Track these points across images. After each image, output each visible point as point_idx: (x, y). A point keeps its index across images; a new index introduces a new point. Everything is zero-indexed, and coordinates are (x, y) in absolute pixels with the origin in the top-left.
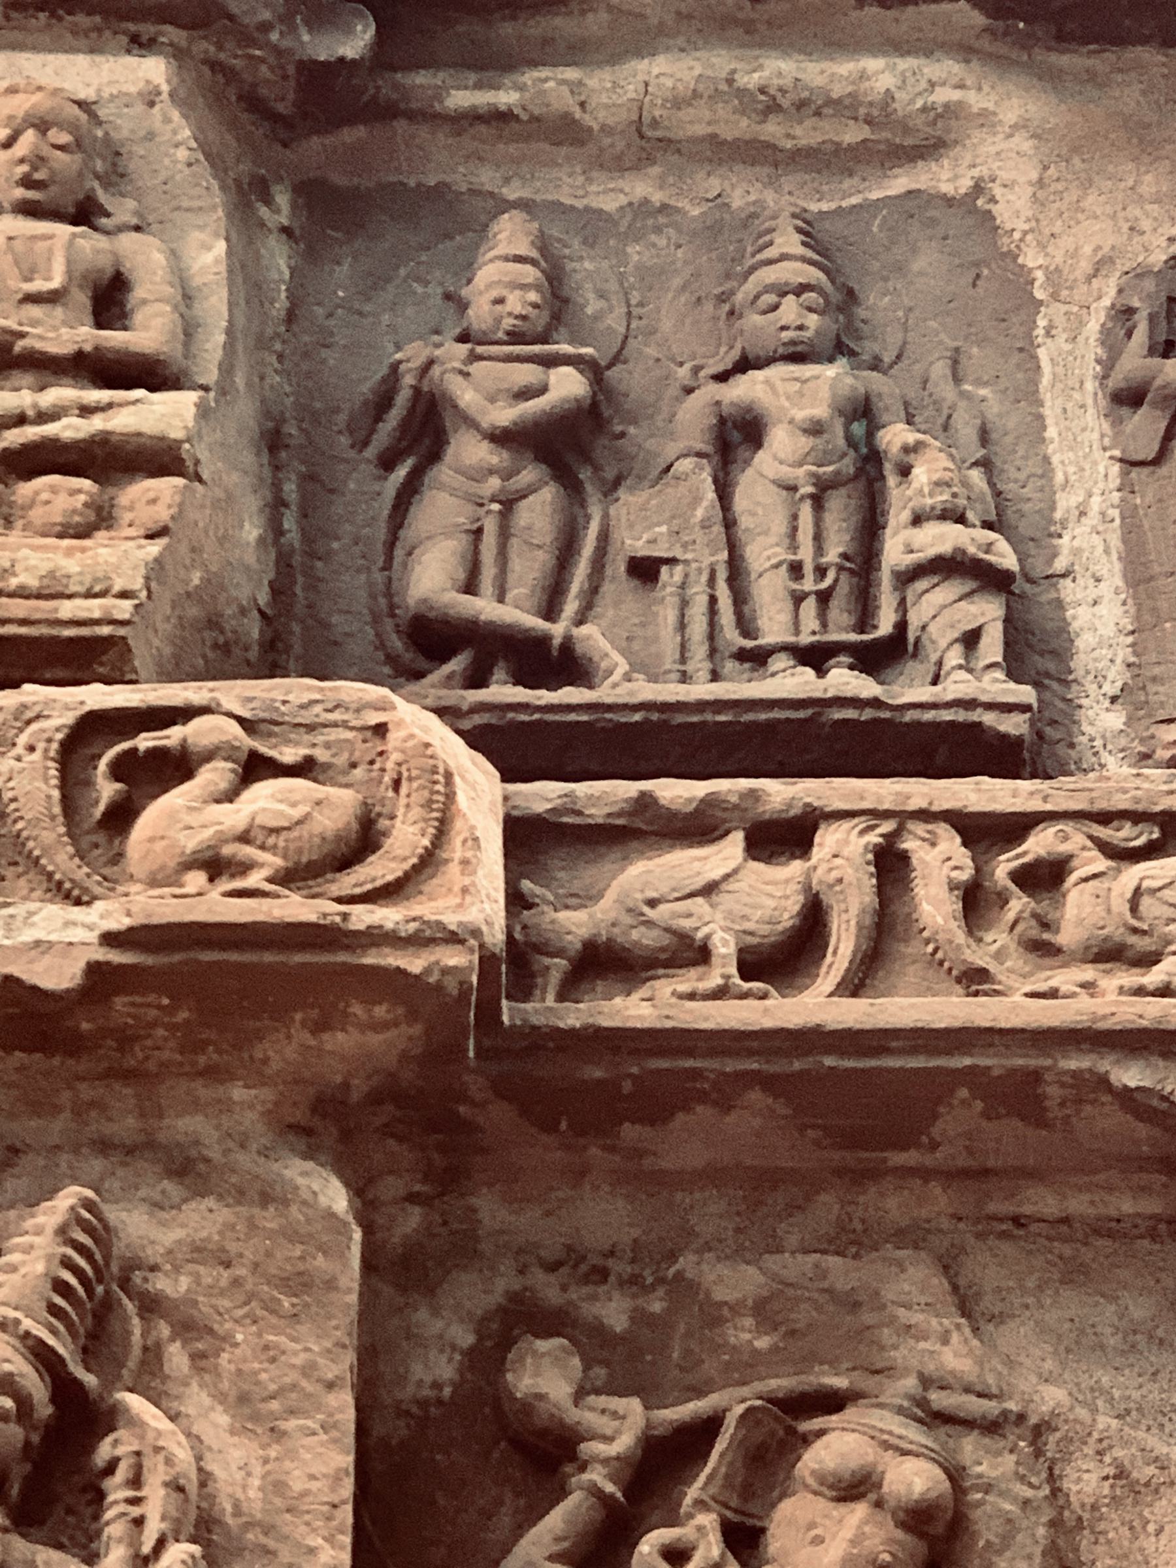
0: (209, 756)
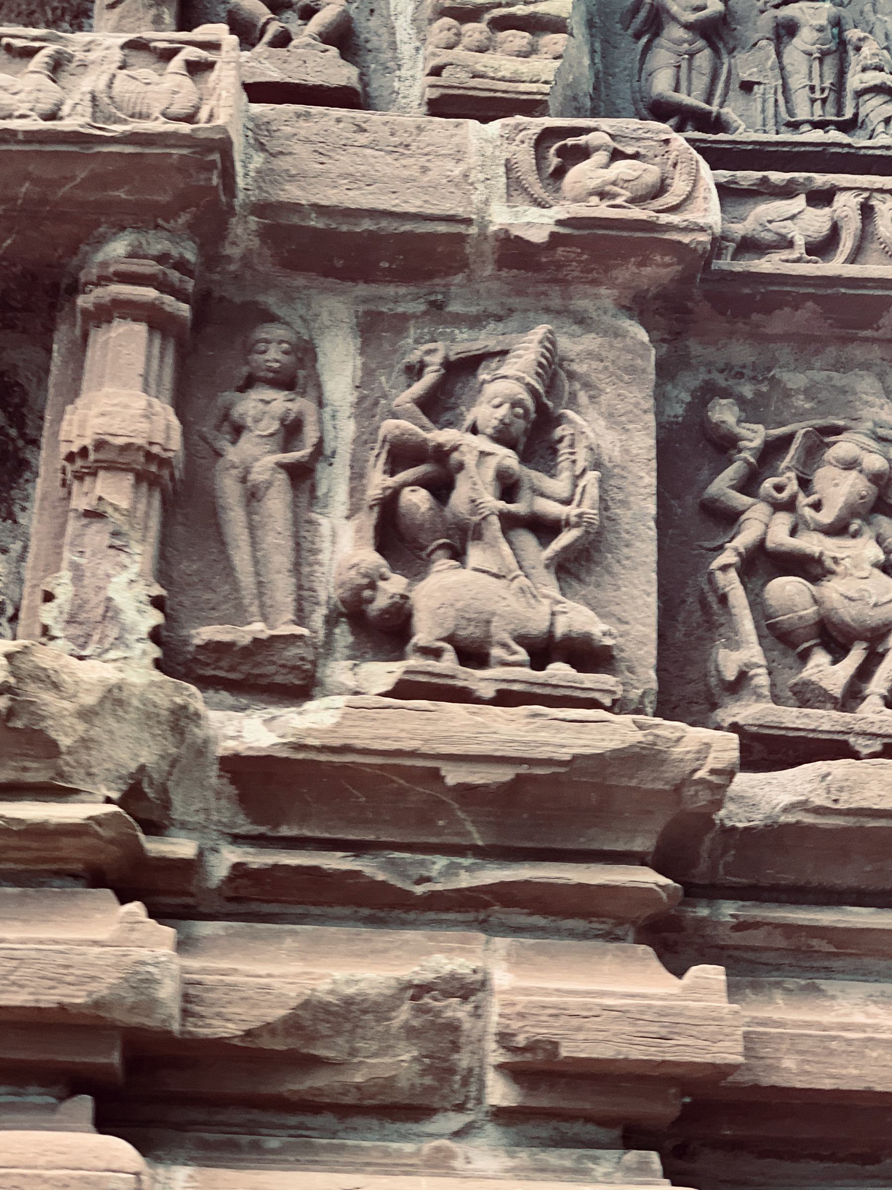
0: (597, 149)
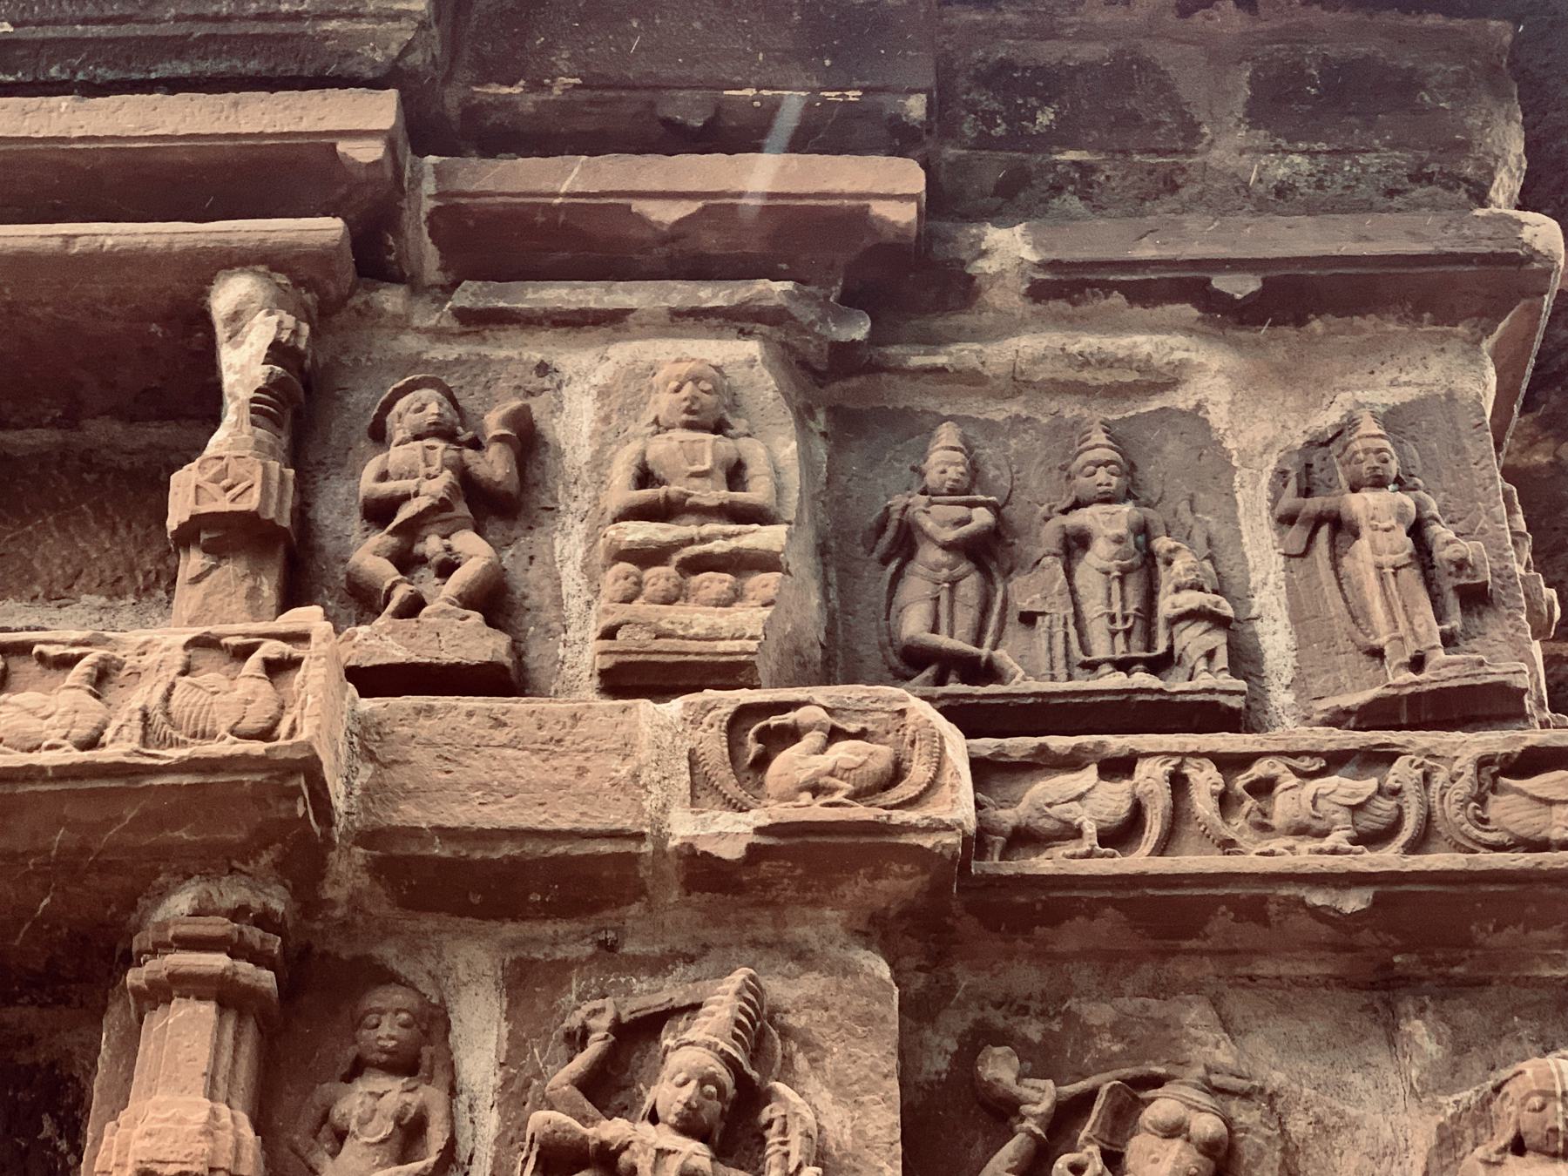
0: (809, 729)
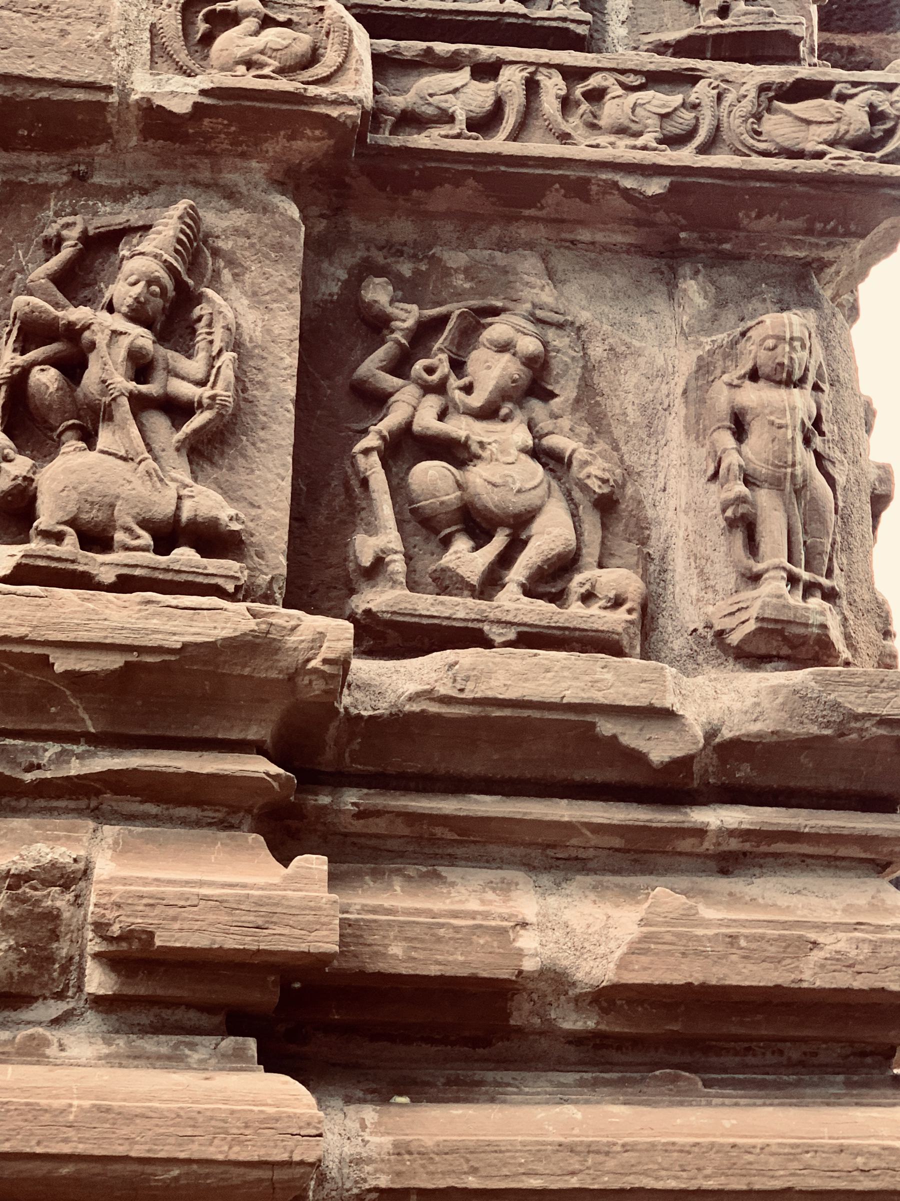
0: (247, 15)
